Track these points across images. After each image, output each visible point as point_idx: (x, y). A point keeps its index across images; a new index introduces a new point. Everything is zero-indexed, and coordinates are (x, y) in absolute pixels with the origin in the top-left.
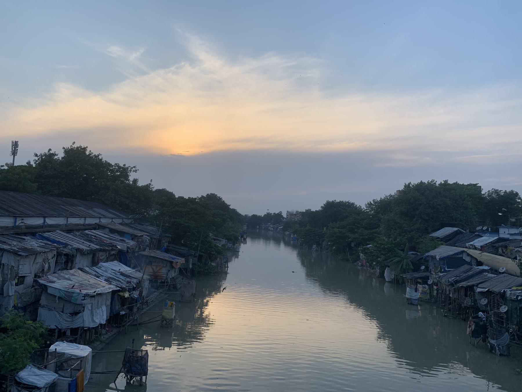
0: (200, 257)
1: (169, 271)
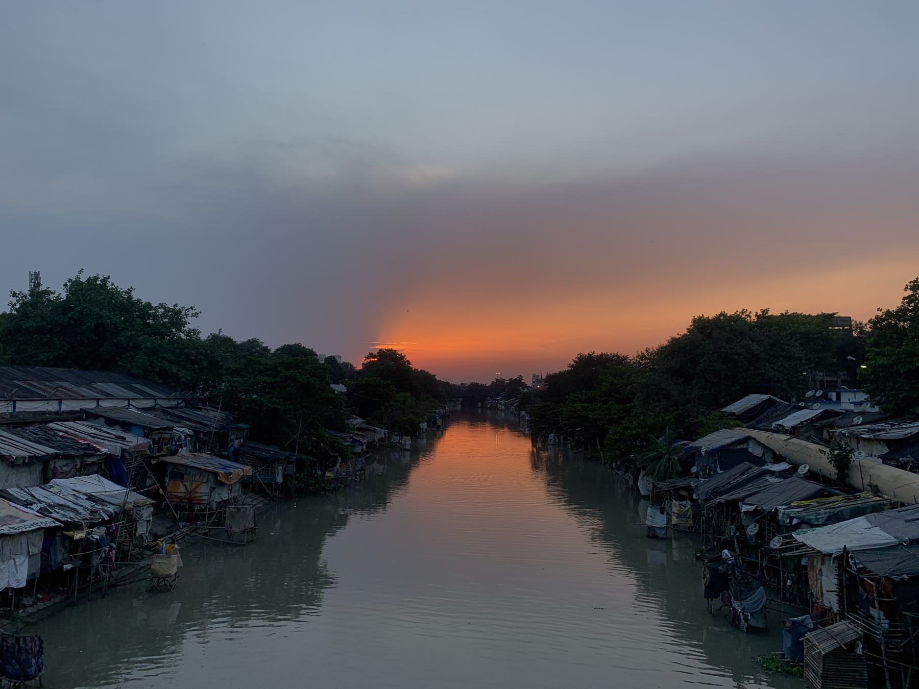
0: (300, 464)
1: (214, 489)
